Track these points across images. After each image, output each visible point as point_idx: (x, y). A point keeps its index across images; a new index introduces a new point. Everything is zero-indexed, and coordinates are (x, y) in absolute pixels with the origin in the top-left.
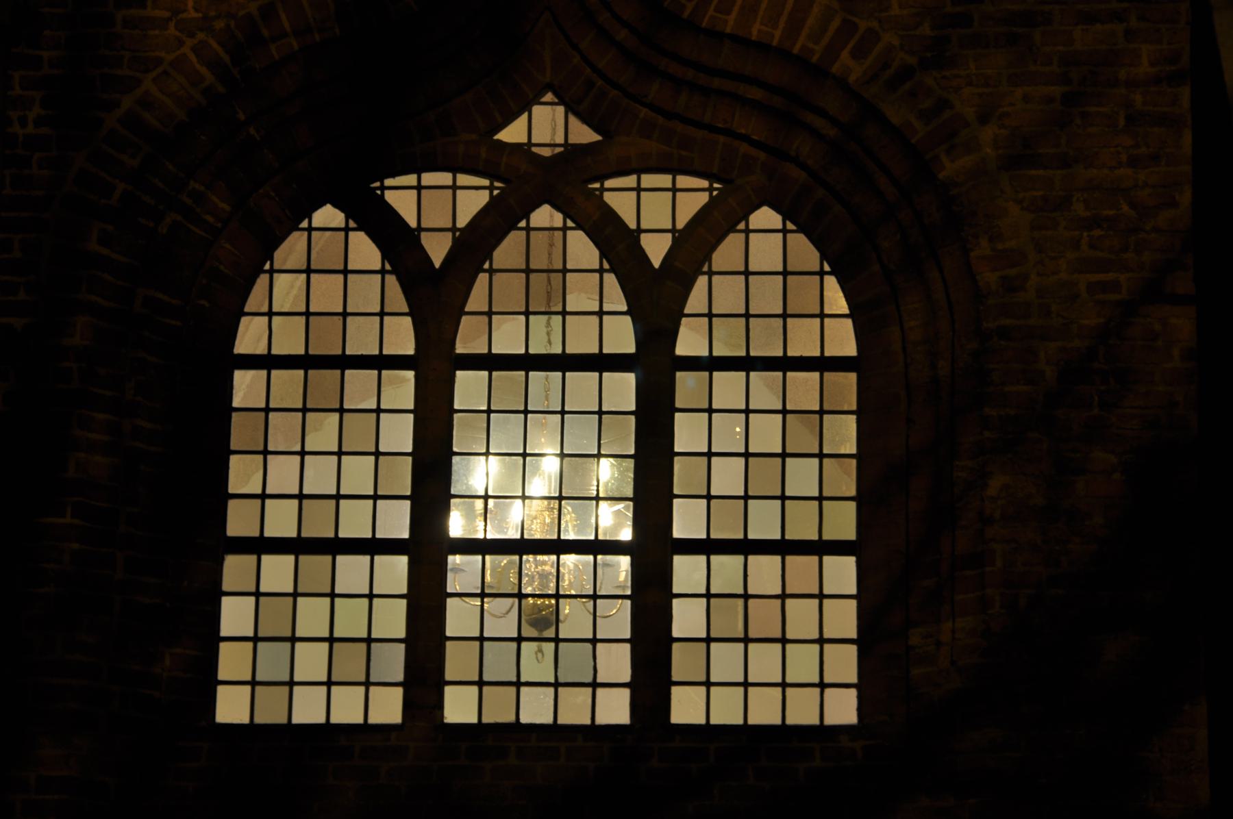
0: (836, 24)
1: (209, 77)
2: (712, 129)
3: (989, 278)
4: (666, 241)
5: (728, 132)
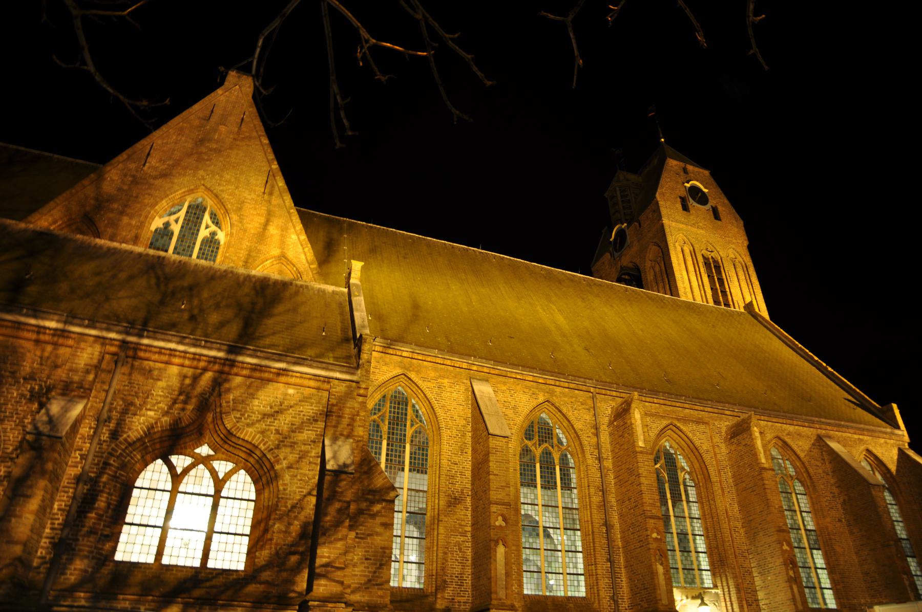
0: (261, 439)
1: (142, 433)
2: (235, 455)
3: (281, 488)
4: (223, 474)
5: (238, 456)
